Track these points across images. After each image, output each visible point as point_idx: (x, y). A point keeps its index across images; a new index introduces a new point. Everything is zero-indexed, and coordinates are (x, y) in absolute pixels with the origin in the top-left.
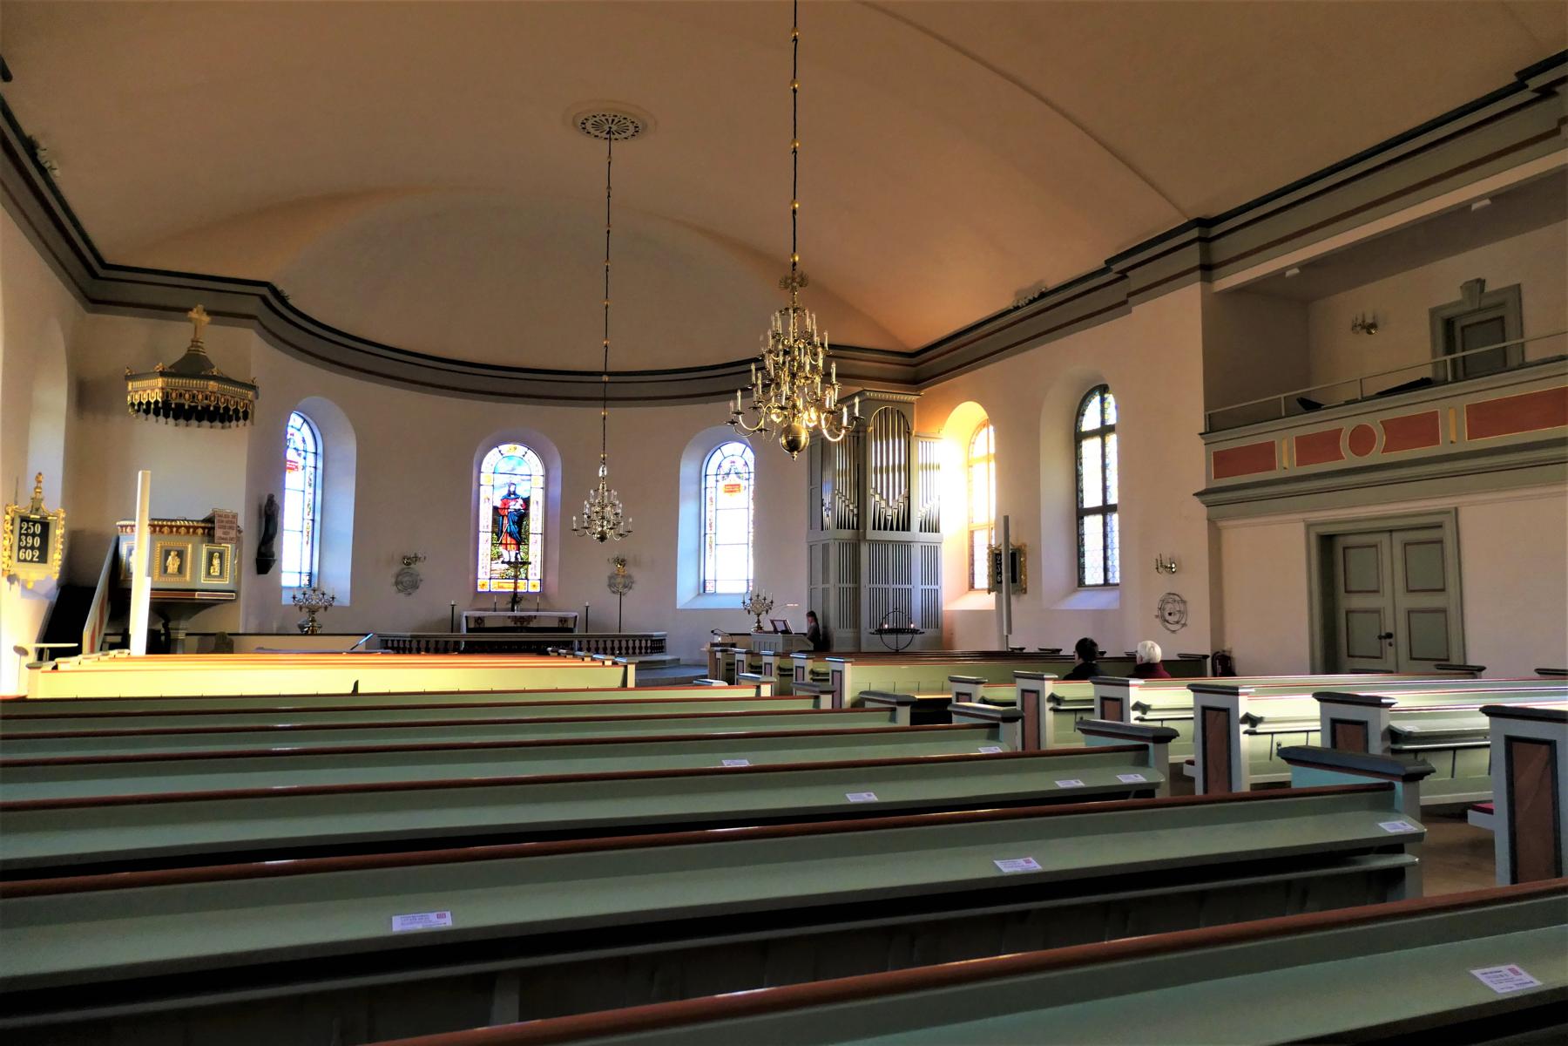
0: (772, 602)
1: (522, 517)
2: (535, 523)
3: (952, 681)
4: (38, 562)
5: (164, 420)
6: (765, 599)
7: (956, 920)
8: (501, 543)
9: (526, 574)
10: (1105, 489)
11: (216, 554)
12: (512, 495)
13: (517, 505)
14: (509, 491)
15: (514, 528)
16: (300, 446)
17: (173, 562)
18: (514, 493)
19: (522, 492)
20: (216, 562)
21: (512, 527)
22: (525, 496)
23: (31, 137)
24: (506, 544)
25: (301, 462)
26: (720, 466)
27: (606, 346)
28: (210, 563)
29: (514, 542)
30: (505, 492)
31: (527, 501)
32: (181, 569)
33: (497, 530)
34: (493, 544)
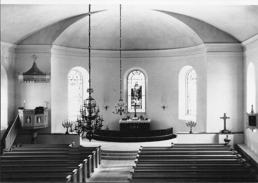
0: (72, 124)
1: (140, 91)
2: (143, 93)
3: (224, 114)
4: (96, 148)
5: (31, 82)
6: (70, 123)
7: (160, 164)
8: (134, 99)
10: (36, 127)
11: (39, 117)
13: (137, 88)
15: (137, 95)
16: (76, 78)
17: (28, 120)
18: (137, 85)
19: (140, 85)
20: (39, 119)
22: (140, 85)
23: (9, 52)
24: (135, 99)
25: (76, 83)
26: (191, 76)
27: (120, 40)
28: (37, 120)
29: (137, 98)
31: (141, 88)
32: (30, 122)
33: (133, 95)
34: (132, 99)
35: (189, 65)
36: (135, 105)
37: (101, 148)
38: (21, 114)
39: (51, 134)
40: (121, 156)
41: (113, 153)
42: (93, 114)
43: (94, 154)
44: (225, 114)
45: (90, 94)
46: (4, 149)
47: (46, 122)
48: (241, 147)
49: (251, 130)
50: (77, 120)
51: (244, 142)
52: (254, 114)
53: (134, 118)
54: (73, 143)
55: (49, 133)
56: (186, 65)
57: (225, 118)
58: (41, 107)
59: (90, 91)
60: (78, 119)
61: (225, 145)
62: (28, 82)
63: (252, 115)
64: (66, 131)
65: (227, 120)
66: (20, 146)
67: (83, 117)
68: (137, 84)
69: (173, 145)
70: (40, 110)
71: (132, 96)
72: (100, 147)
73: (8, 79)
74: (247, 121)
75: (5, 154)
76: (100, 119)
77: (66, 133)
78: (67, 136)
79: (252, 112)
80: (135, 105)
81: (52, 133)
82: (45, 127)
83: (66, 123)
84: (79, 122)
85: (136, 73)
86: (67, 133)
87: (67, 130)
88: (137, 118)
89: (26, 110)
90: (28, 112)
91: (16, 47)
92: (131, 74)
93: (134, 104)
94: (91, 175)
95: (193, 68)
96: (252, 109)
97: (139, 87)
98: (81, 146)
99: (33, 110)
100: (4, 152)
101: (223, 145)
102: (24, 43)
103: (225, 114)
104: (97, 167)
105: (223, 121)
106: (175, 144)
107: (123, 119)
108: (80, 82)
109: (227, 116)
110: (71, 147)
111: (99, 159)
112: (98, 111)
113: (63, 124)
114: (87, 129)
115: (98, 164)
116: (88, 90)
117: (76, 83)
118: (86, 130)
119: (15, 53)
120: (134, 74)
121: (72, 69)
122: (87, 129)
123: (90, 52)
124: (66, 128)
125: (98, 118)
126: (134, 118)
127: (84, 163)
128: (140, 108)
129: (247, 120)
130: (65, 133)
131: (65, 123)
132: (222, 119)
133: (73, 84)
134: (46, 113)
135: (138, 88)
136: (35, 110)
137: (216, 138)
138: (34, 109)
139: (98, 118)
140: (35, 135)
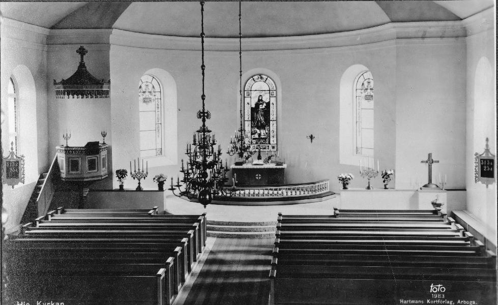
4: (199, 216)
9: (269, 141)
12: (260, 101)
14: (259, 99)
18: (262, 100)
21: (261, 118)
30: (256, 100)
31: (268, 104)
34: (252, 127)
35: (360, 63)
36: (257, 137)
37: (206, 216)
38: (61, 158)
39: (112, 191)
40: (240, 230)
41: (227, 225)
42: (210, 159)
43: (197, 228)
44: (430, 155)
45: (204, 121)
46: (37, 218)
47: (104, 169)
48: (459, 215)
49: (485, 185)
50: (181, 170)
51: (465, 208)
52: (490, 155)
53: (256, 162)
54: (155, 207)
55: (110, 189)
56: (354, 63)
57: (430, 161)
58: (90, 142)
59: (204, 116)
60: (183, 168)
61: (435, 212)
62: (71, 96)
63: (485, 158)
64: (137, 185)
65: (434, 165)
66: (63, 212)
67: (192, 165)
68: (260, 98)
69: (337, 212)
70: (93, 148)
71: (251, 121)
72: (204, 215)
73: (36, 91)
74: (473, 167)
75: (40, 226)
76: (222, 168)
77: (137, 189)
78: (139, 193)
79: (487, 151)
80: (257, 137)
81: (114, 189)
82: (103, 178)
83: (138, 171)
84: (185, 174)
85: (260, 79)
86: (139, 189)
87: (139, 183)
88: (261, 162)
89: (70, 147)
90: (72, 150)
91: (48, 34)
92: (251, 81)
93: (256, 136)
94: (193, 266)
95: (368, 69)
96: (487, 145)
97: (265, 105)
98: (165, 212)
99: (82, 147)
100: (38, 223)
101: (432, 213)
102: (61, 25)
103: (430, 155)
104: (200, 252)
105: (425, 167)
106: (340, 211)
107: (237, 164)
108: (158, 95)
109: (434, 158)
110: (153, 214)
111: (204, 237)
112: (220, 154)
113: (131, 173)
114: (199, 184)
115: (202, 248)
116: (200, 115)
117: (153, 97)
118: (198, 187)
119: (48, 44)
120: (256, 80)
121: (146, 73)
122: (199, 184)
123: (204, 44)
124: (136, 179)
125: (219, 166)
126: (256, 162)
127: (182, 244)
128: (267, 142)
129: (476, 167)
130: (135, 189)
131: (135, 171)
132: (424, 164)
133: (146, 101)
134: (103, 154)
135: (264, 107)
136: (86, 146)
137: (415, 198)
138: (84, 146)
139: (219, 166)
140: (86, 192)
